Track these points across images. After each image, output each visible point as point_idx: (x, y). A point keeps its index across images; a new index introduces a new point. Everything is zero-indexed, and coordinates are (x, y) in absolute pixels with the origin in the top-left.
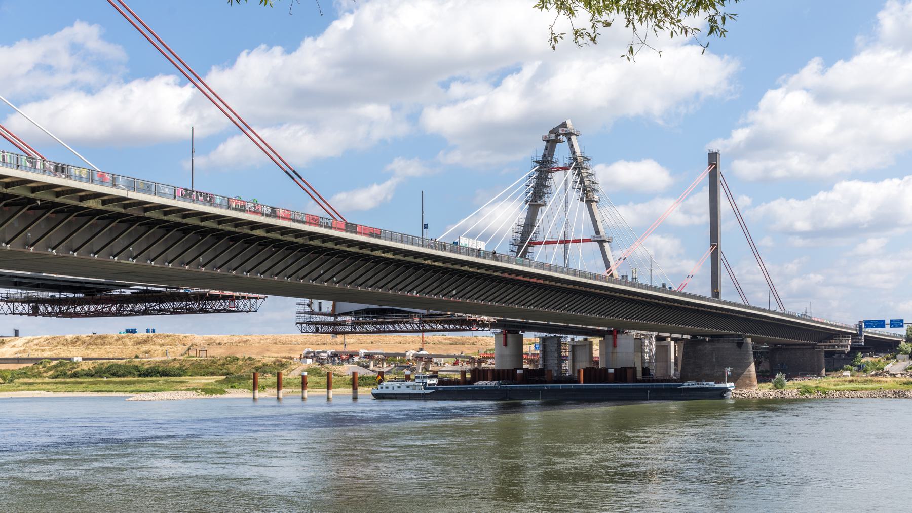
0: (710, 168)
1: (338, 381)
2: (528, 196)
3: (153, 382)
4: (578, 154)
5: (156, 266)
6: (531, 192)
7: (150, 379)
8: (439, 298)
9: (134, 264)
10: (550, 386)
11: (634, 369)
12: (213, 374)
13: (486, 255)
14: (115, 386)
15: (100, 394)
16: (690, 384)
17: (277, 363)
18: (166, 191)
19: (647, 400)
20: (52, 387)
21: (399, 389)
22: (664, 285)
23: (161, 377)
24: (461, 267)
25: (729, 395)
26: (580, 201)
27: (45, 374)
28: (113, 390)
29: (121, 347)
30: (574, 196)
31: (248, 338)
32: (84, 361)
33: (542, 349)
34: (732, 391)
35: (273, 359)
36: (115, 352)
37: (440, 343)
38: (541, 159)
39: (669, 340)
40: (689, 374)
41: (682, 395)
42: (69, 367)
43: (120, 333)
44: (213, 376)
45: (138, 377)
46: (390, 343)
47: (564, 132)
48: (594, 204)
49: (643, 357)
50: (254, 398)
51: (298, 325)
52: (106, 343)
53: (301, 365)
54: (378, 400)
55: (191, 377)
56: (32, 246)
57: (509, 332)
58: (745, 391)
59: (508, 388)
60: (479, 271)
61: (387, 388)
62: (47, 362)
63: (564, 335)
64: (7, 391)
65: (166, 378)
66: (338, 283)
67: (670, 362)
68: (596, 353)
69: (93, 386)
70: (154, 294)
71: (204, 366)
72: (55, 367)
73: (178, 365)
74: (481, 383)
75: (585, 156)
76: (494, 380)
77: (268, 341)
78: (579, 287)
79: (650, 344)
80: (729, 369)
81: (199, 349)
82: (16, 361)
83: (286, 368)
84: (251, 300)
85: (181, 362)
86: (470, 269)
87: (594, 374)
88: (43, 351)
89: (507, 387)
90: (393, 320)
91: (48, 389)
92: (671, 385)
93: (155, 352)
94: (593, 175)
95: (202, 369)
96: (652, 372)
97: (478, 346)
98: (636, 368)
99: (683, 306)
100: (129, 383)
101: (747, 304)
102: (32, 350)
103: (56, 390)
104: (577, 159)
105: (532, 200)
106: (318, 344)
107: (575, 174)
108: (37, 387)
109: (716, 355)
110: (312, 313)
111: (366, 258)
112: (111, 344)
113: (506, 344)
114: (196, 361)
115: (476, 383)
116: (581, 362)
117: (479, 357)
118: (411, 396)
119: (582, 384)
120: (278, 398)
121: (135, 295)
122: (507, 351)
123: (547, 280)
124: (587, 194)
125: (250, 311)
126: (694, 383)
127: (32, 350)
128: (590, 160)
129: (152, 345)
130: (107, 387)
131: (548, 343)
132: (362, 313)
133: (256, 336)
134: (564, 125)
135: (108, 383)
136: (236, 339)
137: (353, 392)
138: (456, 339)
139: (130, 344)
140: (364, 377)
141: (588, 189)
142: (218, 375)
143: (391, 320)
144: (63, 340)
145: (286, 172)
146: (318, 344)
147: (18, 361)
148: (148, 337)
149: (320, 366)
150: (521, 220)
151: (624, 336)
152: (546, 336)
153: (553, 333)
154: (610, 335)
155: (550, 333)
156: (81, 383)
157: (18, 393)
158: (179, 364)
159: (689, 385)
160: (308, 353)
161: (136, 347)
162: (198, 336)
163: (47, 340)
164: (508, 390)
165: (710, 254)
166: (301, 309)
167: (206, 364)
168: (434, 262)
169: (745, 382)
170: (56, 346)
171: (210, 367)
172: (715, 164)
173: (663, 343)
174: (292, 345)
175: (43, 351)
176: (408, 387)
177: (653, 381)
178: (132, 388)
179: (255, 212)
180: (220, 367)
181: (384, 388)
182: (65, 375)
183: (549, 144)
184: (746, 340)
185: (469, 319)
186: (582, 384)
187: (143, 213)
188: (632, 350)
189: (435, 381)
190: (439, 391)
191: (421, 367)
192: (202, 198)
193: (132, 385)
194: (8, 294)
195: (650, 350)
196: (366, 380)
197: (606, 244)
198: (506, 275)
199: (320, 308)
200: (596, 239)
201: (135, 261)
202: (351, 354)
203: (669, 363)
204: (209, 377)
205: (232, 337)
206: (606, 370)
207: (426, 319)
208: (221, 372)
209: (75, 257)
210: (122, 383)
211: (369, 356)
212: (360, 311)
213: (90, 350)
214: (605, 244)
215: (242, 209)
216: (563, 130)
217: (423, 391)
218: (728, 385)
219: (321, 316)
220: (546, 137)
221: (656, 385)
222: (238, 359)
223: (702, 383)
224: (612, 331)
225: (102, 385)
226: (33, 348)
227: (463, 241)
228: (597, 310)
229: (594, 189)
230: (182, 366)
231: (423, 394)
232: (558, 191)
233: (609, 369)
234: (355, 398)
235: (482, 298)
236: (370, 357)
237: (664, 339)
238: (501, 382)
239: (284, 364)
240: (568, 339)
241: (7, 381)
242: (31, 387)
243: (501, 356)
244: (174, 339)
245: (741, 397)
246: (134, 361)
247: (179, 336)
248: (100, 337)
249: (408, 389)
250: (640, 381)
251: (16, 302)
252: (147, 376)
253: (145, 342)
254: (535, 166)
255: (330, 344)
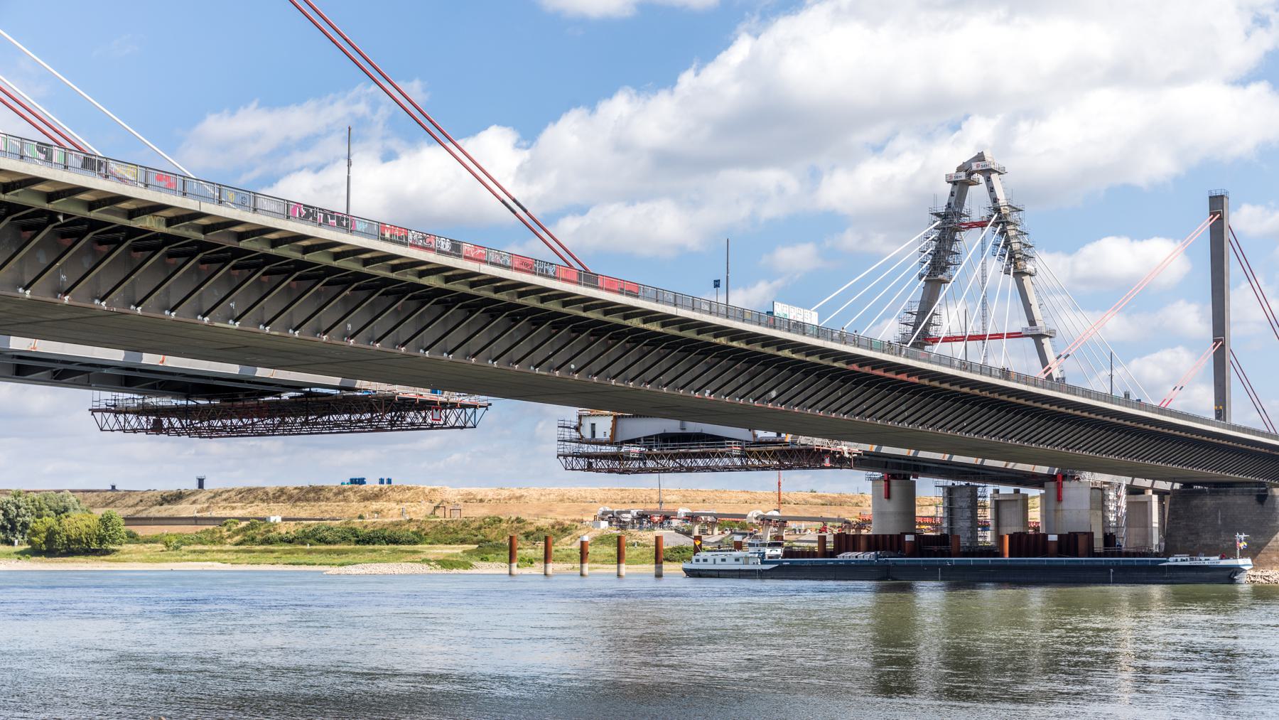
0: (1211, 220)
1: (642, 554)
2: (923, 267)
3: (374, 551)
4: (1002, 200)
5: (272, 333)
6: (929, 262)
7: (371, 547)
8: (747, 403)
9: (237, 330)
10: (955, 561)
11: (1090, 535)
12: (463, 541)
13: (820, 332)
14: (319, 556)
15: (296, 568)
16: (1179, 559)
17: (557, 527)
18: (273, 207)
19: (1110, 583)
20: (231, 557)
22: (1127, 395)
23: (388, 544)
25: (1242, 578)
26: (1005, 274)
27: (229, 540)
28: (315, 561)
29: (342, 503)
30: (995, 267)
31: (523, 492)
32: (284, 522)
33: (946, 505)
34: (1248, 572)
35: (552, 521)
36: (332, 512)
38: (944, 211)
39: (1150, 492)
40: (1179, 545)
42: (262, 529)
43: (342, 484)
44: (463, 544)
45: (355, 545)
47: (980, 168)
48: (1026, 279)
49: (1105, 518)
50: (510, 574)
51: (561, 458)
52: (322, 498)
53: (592, 530)
54: (692, 579)
55: (430, 546)
56: (66, 293)
57: (894, 477)
58: (1270, 572)
59: (891, 563)
60: (808, 359)
61: (705, 560)
62: (235, 523)
63: (981, 484)
64: (167, 561)
65: (395, 546)
66: (577, 372)
67: (1152, 527)
68: (1035, 515)
69: (288, 556)
70: (319, 398)
71: (452, 530)
72: (244, 530)
73: (415, 529)
74: (850, 554)
75: (1013, 205)
76: (869, 550)
77: (552, 496)
78: (981, 391)
79: (1118, 497)
80: (1243, 536)
81: (449, 507)
82: (193, 522)
83: (570, 534)
84: (467, 409)
85: (418, 523)
86: (794, 356)
87: (1027, 543)
88: (233, 509)
89: (888, 561)
90: (702, 450)
91: (225, 560)
92: (1148, 561)
93: (390, 512)
94: (1025, 234)
95: (447, 534)
97: (864, 508)
98: (1093, 533)
99: (1160, 429)
100: (339, 553)
101: (1272, 431)
102: (219, 508)
103: (236, 561)
104: (1000, 210)
105: (930, 273)
106: (625, 503)
107: (997, 232)
108: (210, 556)
109: (1221, 515)
110: (581, 440)
111: (618, 333)
112: (328, 499)
113: (888, 496)
114: (441, 522)
115: (842, 555)
116: (1010, 526)
117: (858, 520)
119: (1007, 557)
120: (546, 574)
121: (293, 400)
122: (891, 507)
123: (925, 378)
124: (1016, 264)
125: (465, 427)
126: (1184, 558)
127: (219, 508)
128: (1020, 210)
129: (386, 501)
130: (307, 558)
131: (956, 495)
132: (657, 441)
133: (534, 490)
134: (980, 157)
135: (310, 552)
136: (505, 493)
138: (830, 497)
139: (355, 500)
141: (1017, 256)
142: (469, 544)
143: (698, 450)
144: (261, 494)
145: (503, 202)
146: (625, 503)
147: (196, 521)
148: (381, 490)
149: (619, 532)
150: (913, 304)
151: (1074, 483)
152: (953, 484)
153: (963, 479)
154: (1054, 483)
155: (958, 479)
156: (272, 552)
157: (182, 564)
158: (416, 527)
159: (1176, 561)
160: (605, 513)
161: (362, 504)
162: (451, 489)
163: (240, 493)
164: (888, 566)
166: (565, 433)
167: (455, 526)
168: (732, 340)
169: (1270, 557)
170: (252, 502)
171: (459, 532)
172: (1220, 213)
173: (1140, 498)
174: (586, 504)
175: (233, 508)
176: (737, 560)
177: (1120, 554)
178: (344, 559)
179: (423, 248)
180: (474, 532)
182: (253, 540)
183: (956, 188)
184: (1272, 491)
186: (1007, 557)
187: (236, 242)
188: (1087, 505)
189: (779, 551)
190: (784, 566)
191: (769, 535)
192: (335, 221)
193: (344, 555)
194: (115, 400)
195: (1118, 507)
196: (683, 552)
197: (1046, 341)
199: (593, 433)
200: (1029, 333)
201: (237, 323)
202: (667, 514)
203: (1149, 529)
204: (456, 546)
205: (500, 491)
207: (752, 449)
208: (475, 539)
209: (139, 315)
210: (329, 552)
211: (692, 518)
212: (652, 436)
213: (298, 508)
214: (1044, 341)
215: (402, 242)
216: (978, 166)
217: (760, 567)
218: (1240, 562)
219: (595, 446)
220: (951, 177)
222: (500, 521)
223: (1198, 558)
224: (1055, 476)
225: (301, 555)
226: (219, 505)
227: (781, 310)
228: (1015, 432)
229: (1027, 256)
230: (420, 529)
231: (759, 570)
232: (969, 256)
233: (1049, 536)
234: (659, 575)
235: (821, 405)
237: (1141, 491)
238: (878, 553)
239: (566, 529)
240: (987, 491)
241: (171, 548)
242: (202, 557)
244: (417, 494)
245: (1264, 581)
246: (354, 523)
247: (424, 488)
248: (314, 490)
250: (1099, 555)
251: (129, 413)
252: (368, 543)
253: (376, 496)
254: (934, 222)
255: (642, 502)
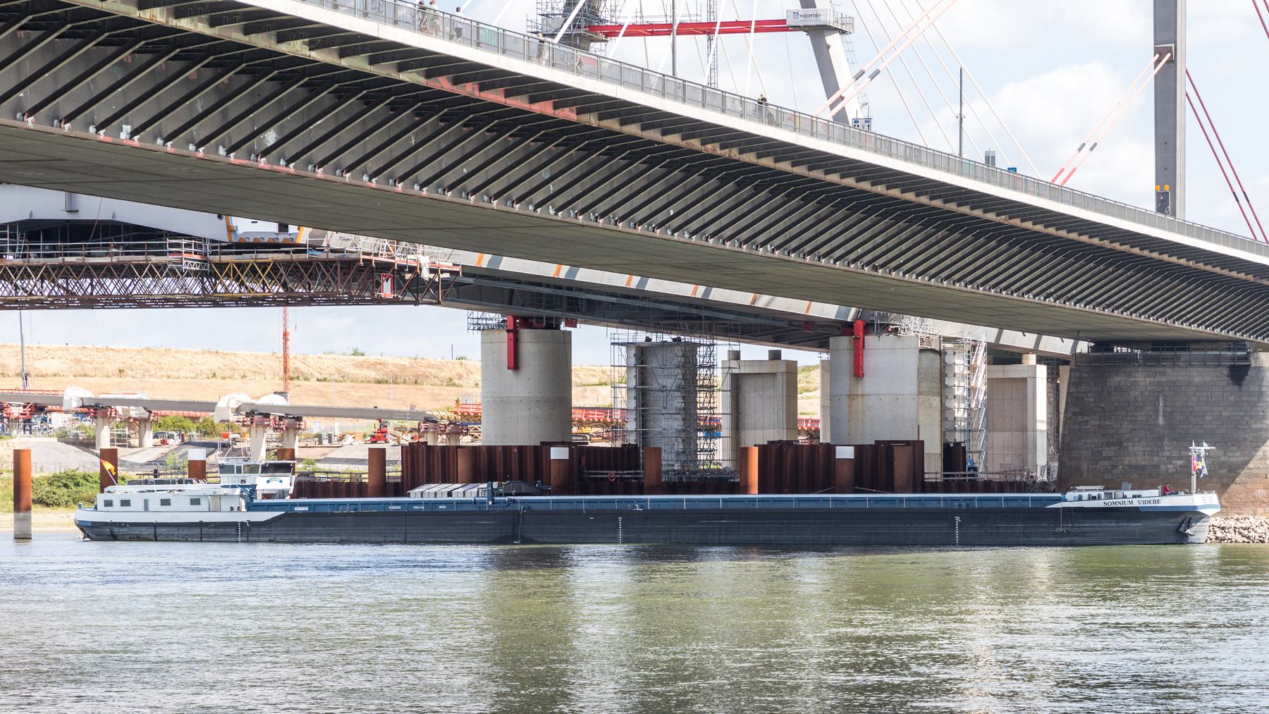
10: (652, 501)
11: (917, 447)
16: (1085, 495)
21: (166, 508)
22: (990, 159)
24: (280, 41)
37: (344, 377)
39: (1032, 359)
41: (1057, 530)
46: (182, 374)
49: (944, 410)
57: (527, 322)
58: (1252, 521)
61: (125, 503)
63: (704, 341)
67: (1035, 430)
76: (475, 478)
78: (703, 143)
79: (972, 368)
89: (514, 501)
90: (115, 259)
96: (975, 459)
97: (465, 390)
98: (922, 442)
101: (1260, 238)
113: (515, 364)
117: (452, 416)
118: (205, 530)
119: (754, 493)
122: (523, 386)
126: (1095, 494)
131: (653, 363)
137: (17, 520)
140: (72, 477)
151: (887, 340)
152: (648, 340)
155: (657, 328)
159: (1080, 499)
164: (516, 513)
165: (1150, 82)
168: (179, 15)
169: (1252, 491)
173: (1013, 371)
176: (195, 501)
177: (974, 486)
181: (117, 504)
184: (1257, 358)
185: (367, 262)
188: (911, 386)
189: (285, 483)
195: (971, 390)
196: (77, 484)
198: (443, 84)
200: (801, 22)
202: (40, 402)
203: (1030, 434)
206: (830, 449)
221: (980, 499)
223: (1120, 493)
228: (772, 231)
234: (23, 537)
236: (99, 412)
238: (495, 485)
243: (500, 402)
249: (196, 507)
250: (934, 487)
